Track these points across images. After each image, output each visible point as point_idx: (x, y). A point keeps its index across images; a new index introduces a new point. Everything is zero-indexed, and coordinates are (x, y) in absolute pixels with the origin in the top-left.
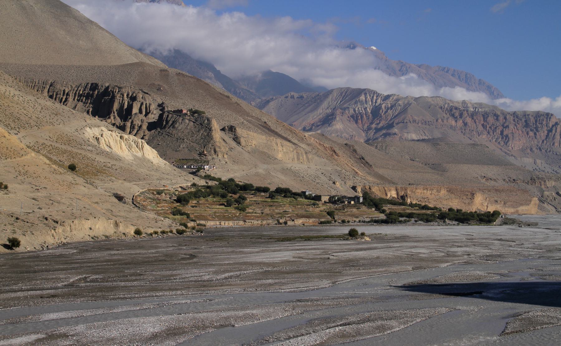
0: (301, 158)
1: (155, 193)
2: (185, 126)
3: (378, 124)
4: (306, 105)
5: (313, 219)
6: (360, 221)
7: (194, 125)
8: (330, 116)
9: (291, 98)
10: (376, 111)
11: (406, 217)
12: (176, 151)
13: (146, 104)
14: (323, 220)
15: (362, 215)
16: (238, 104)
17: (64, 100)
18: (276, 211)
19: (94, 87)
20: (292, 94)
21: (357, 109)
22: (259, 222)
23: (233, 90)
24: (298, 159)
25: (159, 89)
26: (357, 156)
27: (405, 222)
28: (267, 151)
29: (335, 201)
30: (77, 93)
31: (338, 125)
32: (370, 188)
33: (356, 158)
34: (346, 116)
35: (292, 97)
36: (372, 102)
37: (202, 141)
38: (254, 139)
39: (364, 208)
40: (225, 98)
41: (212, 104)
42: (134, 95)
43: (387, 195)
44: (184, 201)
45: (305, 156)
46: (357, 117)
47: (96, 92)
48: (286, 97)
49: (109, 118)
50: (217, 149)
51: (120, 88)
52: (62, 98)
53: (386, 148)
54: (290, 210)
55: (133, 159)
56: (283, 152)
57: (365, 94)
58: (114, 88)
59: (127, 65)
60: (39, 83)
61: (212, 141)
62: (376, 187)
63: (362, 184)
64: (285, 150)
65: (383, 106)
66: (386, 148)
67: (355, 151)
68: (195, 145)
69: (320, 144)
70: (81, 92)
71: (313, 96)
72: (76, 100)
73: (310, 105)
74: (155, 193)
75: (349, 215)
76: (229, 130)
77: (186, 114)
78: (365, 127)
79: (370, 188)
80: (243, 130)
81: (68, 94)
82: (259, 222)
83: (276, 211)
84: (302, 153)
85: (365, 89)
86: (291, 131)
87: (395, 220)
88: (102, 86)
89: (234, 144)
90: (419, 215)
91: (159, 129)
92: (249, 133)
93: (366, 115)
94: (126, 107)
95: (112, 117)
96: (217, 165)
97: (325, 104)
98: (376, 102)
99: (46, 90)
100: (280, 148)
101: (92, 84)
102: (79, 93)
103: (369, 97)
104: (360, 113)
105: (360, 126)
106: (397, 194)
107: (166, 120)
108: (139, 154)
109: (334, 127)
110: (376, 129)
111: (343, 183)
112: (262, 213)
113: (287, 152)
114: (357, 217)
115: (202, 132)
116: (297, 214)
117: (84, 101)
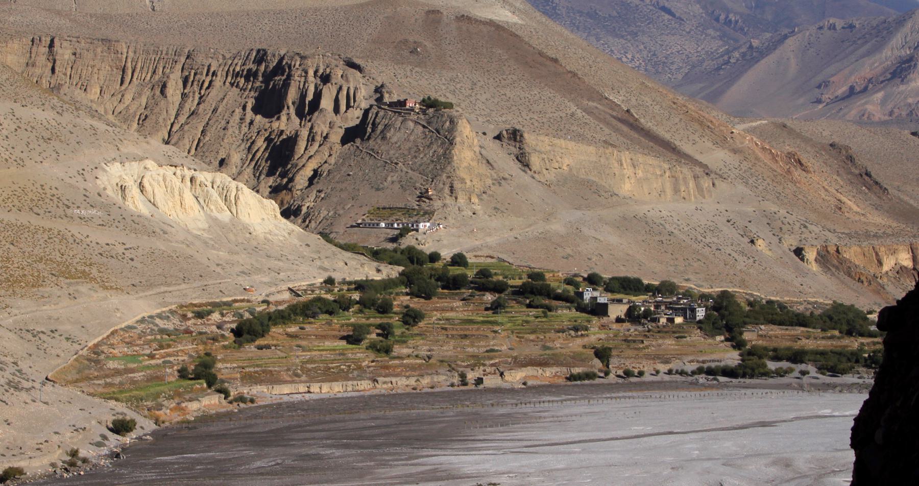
0: (683, 189)
1: (190, 315)
2: (406, 133)
4: (859, 42)
7: (424, 132)
9: (829, 29)
12: (378, 189)
13: (349, 88)
14: (577, 370)
15: (679, 356)
17: (206, 85)
18: (470, 350)
22: (412, 381)
23: (722, 17)
24: (676, 190)
25: (413, 52)
26: (854, 170)
27: (780, 373)
28: (596, 179)
29: (639, 317)
30: (231, 69)
32: (838, 251)
33: (851, 173)
35: (832, 27)
37: (431, 166)
38: (563, 154)
39: (696, 336)
40: (548, 63)
42: (328, 71)
43: (880, 263)
44: (248, 333)
45: (692, 184)
47: (263, 68)
48: (821, 28)
49: (278, 119)
50: (457, 185)
51: (303, 58)
52: (204, 81)
54: (504, 348)
55: (206, 226)
56: (637, 179)
58: (292, 58)
60: (167, 54)
61: (449, 168)
62: (856, 248)
64: (640, 174)
67: (851, 158)
68: (415, 175)
69: (764, 149)
70: (238, 69)
71: (874, 23)
72: (227, 84)
73: (866, 42)
74: (190, 315)
75: (648, 357)
76: (509, 139)
77: (412, 109)
79: (838, 251)
80: (542, 138)
81: (214, 74)
82: (412, 381)
83: (470, 350)
84: (685, 179)
86: (701, 124)
87: (753, 370)
88: (274, 56)
89: (514, 167)
91: (358, 141)
94: (310, 97)
95: (284, 118)
96: (451, 220)
97: (897, 39)
100: (628, 171)
101: (259, 51)
102: (234, 70)
107: (374, 124)
111: (776, 239)
113: (647, 179)
114: (667, 362)
115: (435, 147)
116: (515, 358)
117: (241, 85)
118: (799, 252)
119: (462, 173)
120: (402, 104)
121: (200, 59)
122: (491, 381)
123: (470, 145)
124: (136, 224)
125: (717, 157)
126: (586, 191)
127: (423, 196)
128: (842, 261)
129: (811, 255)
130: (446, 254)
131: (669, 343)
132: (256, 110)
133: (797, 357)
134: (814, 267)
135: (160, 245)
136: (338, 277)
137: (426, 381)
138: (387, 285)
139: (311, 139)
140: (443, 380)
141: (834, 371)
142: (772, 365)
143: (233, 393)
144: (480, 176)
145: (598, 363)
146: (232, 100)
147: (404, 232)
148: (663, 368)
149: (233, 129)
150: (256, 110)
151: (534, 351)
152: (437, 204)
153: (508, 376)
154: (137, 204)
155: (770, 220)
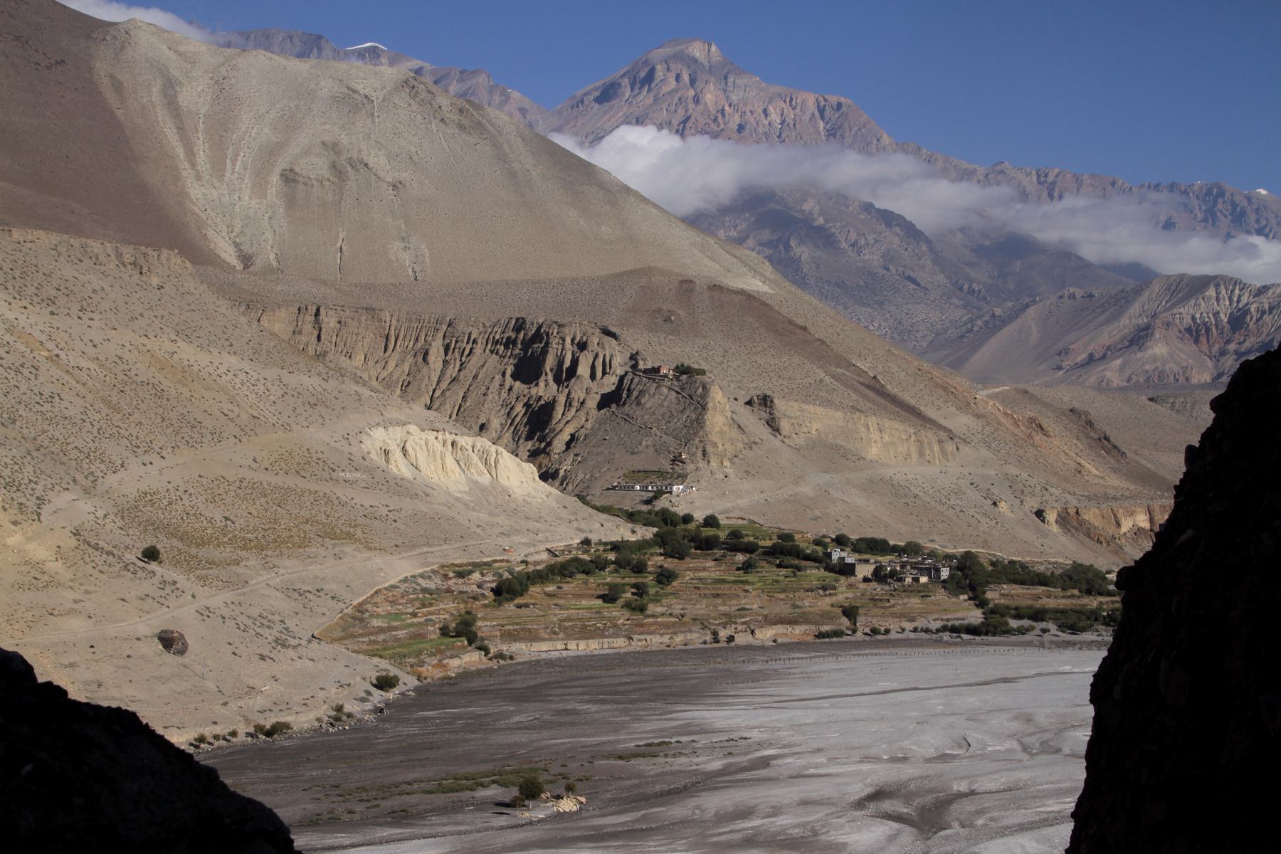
1: (451, 575)
2: (660, 399)
3: (1240, 343)
5: (803, 628)
6: (915, 630)
8: (1142, 330)
10: (1238, 321)
11: (1030, 618)
12: (633, 453)
14: (825, 628)
15: (924, 614)
16: (823, 342)
17: (467, 352)
19: (520, 325)
20: (1071, 290)
21: (1198, 316)
22: (666, 639)
23: (966, 287)
24: (921, 454)
25: (667, 320)
26: (1093, 434)
27: (1022, 631)
29: (885, 576)
31: (1158, 349)
32: (1077, 513)
33: (1091, 438)
34: (1176, 330)
35: (1072, 296)
36: (1230, 299)
37: (685, 431)
39: (940, 595)
40: (798, 331)
41: (765, 345)
43: (1119, 525)
46: (1198, 331)
48: (1061, 297)
49: (537, 385)
50: (710, 449)
53: (1192, 408)
54: (755, 607)
55: (467, 489)
56: (884, 444)
57: (1217, 286)
58: (550, 326)
59: (623, 274)
62: (1094, 510)
63: (1059, 506)
64: (886, 438)
65: (1253, 308)
66: (1192, 408)
70: (497, 337)
71: (1113, 293)
75: (894, 615)
76: (760, 404)
77: (666, 376)
78: (1216, 348)
79: (1077, 513)
81: (475, 341)
82: (666, 639)
83: (722, 608)
84: (929, 443)
85: (1215, 277)
86: (945, 389)
87: (996, 628)
89: (763, 432)
90: (1063, 612)
91: (614, 406)
92: (805, 406)
93: (1217, 326)
95: (542, 384)
97: (1135, 308)
98: (1239, 301)
99: (441, 334)
100: (875, 435)
101: (517, 319)
103: (1224, 291)
104: (1205, 324)
105: (1205, 348)
106: (1152, 520)
107: (629, 390)
108: (485, 479)
109: (1150, 352)
110: (1236, 352)
112: (683, 616)
114: (912, 620)
115: (688, 412)
116: (766, 616)
118: (1040, 514)
119: (714, 437)
120: (656, 370)
121: (460, 326)
122: (742, 639)
123: (722, 411)
124: (399, 487)
125: (961, 422)
126: (833, 455)
127: (677, 459)
128: (1082, 523)
129: (1051, 516)
130: (699, 516)
131: (914, 602)
132: (515, 377)
133: (1038, 615)
134: (1055, 528)
135: (423, 507)
136: (594, 538)
137: (679, 639)
138: (642, 545)
139: (568, 404)
140: (696, 638)
141: (1074, 629)
142: (1014, 623)
143: (493, 650)
144: (732, 441)
145: (845, 621)
146: (492, 367)
147: (658, 494)
148: (909, 626)
149: (493, 394)
150: (515, 377)
151: (784, 609)
152: (690, 467)
153: (758, 634)
154: (400, 467)
155: (1012, 483)
